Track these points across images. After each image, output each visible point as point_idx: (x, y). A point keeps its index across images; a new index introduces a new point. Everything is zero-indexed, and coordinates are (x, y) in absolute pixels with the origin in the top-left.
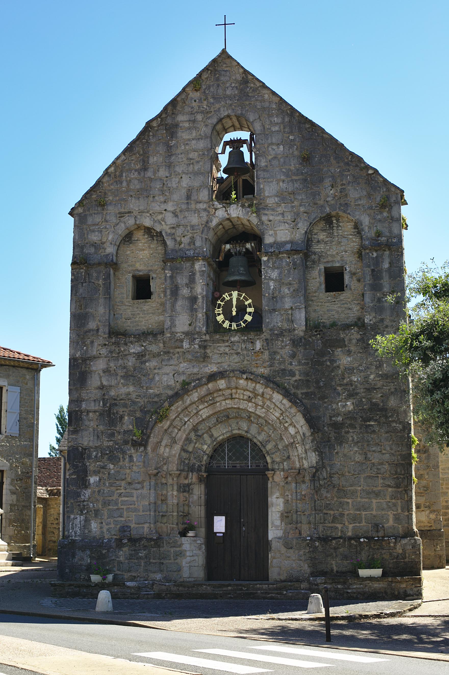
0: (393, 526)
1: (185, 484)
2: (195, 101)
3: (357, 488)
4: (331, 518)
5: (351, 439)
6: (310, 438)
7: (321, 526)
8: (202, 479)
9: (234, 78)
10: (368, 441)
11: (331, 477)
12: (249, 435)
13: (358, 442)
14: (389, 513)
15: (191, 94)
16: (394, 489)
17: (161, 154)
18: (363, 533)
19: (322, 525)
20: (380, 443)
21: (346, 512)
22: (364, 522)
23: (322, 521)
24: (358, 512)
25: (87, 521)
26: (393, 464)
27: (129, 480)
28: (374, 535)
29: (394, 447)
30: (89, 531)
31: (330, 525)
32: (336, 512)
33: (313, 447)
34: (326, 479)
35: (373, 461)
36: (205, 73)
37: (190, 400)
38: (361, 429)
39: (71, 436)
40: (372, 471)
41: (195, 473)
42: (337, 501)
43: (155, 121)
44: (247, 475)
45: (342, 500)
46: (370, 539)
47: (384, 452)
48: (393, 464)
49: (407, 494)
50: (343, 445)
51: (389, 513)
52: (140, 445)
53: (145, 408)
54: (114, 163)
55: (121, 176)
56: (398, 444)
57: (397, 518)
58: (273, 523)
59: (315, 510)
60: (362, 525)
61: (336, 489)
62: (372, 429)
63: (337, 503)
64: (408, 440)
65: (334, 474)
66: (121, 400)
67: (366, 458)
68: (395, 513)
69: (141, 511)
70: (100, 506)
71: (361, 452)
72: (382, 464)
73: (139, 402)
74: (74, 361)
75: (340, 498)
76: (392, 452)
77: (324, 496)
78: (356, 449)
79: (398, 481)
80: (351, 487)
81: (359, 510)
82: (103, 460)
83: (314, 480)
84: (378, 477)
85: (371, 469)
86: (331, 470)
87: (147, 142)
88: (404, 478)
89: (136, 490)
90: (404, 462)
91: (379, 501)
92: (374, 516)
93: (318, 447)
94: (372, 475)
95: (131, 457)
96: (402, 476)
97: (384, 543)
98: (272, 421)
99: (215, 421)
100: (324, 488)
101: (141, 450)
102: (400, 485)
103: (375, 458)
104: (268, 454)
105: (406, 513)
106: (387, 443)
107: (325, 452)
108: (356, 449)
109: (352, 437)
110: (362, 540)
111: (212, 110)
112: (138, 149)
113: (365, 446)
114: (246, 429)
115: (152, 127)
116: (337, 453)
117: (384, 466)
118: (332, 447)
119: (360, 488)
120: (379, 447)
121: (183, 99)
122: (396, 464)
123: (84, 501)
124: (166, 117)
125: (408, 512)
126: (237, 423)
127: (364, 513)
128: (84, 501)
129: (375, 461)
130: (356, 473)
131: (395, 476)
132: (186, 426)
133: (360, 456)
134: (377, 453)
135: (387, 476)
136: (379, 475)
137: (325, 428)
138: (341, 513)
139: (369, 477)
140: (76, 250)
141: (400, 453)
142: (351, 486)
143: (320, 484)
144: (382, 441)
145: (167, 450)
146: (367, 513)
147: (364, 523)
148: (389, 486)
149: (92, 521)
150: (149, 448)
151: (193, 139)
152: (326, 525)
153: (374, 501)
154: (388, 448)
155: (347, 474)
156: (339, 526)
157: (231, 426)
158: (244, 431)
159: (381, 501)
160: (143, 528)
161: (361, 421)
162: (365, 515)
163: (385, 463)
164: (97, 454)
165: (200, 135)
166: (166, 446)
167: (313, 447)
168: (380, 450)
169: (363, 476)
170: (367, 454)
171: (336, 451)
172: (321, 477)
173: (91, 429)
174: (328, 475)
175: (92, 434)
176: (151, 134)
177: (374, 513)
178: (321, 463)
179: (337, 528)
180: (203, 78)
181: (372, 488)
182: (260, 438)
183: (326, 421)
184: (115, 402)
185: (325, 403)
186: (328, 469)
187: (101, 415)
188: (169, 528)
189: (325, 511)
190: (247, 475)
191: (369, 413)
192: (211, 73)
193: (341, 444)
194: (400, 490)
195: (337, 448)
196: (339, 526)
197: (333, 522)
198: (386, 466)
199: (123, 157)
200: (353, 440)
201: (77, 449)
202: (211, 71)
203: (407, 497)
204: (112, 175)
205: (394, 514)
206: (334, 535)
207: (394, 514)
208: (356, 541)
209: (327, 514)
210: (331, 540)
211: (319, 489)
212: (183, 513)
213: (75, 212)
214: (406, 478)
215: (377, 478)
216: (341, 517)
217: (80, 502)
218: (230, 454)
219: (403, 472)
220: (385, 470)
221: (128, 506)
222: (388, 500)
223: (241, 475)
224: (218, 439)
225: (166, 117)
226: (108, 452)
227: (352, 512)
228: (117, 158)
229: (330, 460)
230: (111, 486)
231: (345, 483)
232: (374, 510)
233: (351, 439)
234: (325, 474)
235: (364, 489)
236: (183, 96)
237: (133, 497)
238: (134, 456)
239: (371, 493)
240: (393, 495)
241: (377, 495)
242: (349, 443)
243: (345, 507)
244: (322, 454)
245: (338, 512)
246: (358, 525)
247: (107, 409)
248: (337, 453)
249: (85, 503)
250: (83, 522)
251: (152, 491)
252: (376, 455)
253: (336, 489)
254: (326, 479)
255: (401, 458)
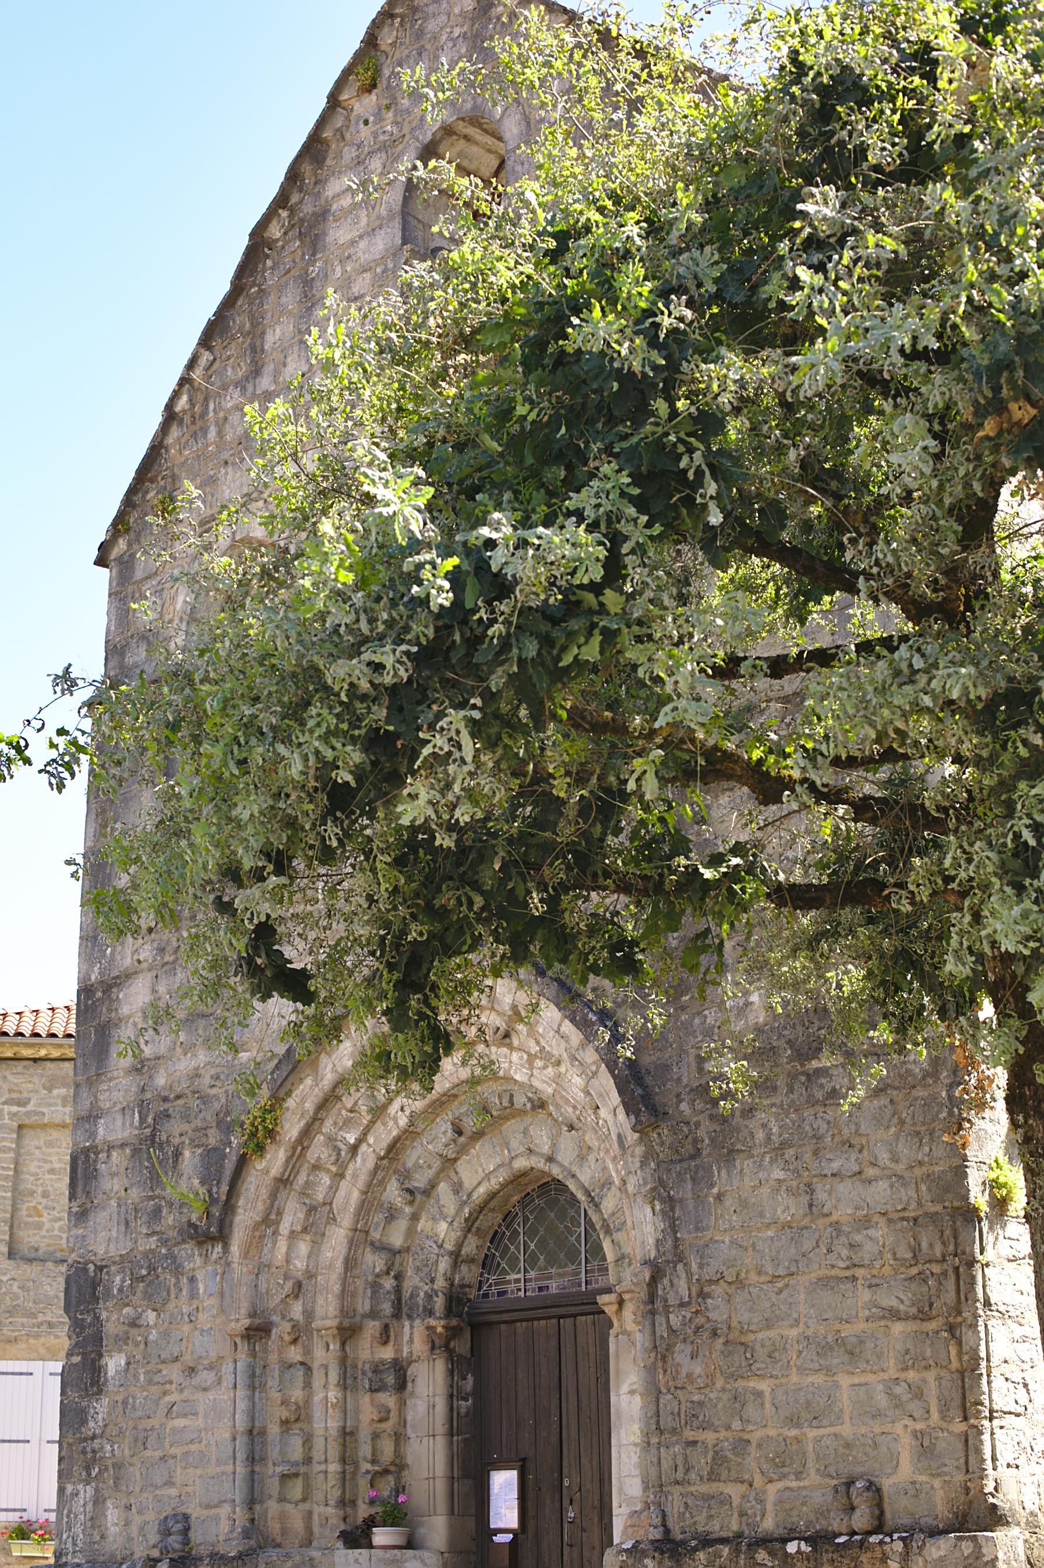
0: (913, 1483)
1: (382, 1362)
2: (366, 123)
3: (786, 1332)
4: (702, 1462)
5: (760, 1135)
6: (639, 1150)
7: (676, 1495)
8: (437, 1341)
9: (457, 11)
10: (818, 1138)
11: (703, 1295)
12: (556, 1171)
13: (784, 1145)
14: (898, 1428)
15: (357, 106)
16: (911, 1326)
17: (290, 312)
18: (812, 1517)
19: (679, 1488)
20: (855, 1141)
21: (756, 1436)
22: (812, 1472)
23: (680, 1475)
24: (794, 1432)
25: (98, 1501)
26: (903, 1219)
27: (187, 1358)
28: (835, 1526)
29: (904, 1149)
30: (103, 1537)
31: (704, 1488)
32: (723, 1434)
33: (645, 1184)
34: (689, 1303)
35: (834, 1218)
36: (386, 30)
37: (334, 1070)
38: (791, 1090)
39: (74, 1232)
40: (832, 1258)
41: (417, 1322)
42: (724, 1389)
43: (274, 222)
44: (575, 1316)
45: (741, 1383)
46: (819, 1540)
47: (870, 1172)
48: (903, 1219)
49: (960, 1344)
50: (738, 1163)
51: (898, 1428)
52: (213, 1239)
53: (228, 1113)
54: (184, 381)
55: (204, 413)
56: (918, 1133)
57: (925, 1449)
58: (621, 1490)
59: (660, 1431)
60: (806, 1483)
61: (721, 1340)
62: (828, 1088)
63: (725, 1397)
64: (951, 1113)
65: (711, 1282)
66: (178, 1097)
67: (811, 1206)
68: (919, 1426)
69: (213, 1461)
70: (127, 1452)
71: (794, 1183)
72: (865, 1223)
73: (216, 1097)
74: (87, 998)
75: (734, 1377)
76: (900, 1168)
77: (684, 1372)
78: (778, 1174)
79: (925, 1289)
80: (769, 1327)
81: (793, 1421)
82: (134, 1299)
83: (653, 1313)
84: (854, 1278)
85: (830, 1251)
86: (701, 1266)
87: (261, 291)
88: (945, 1273)
89: (205, 1390)
90: (938, 1208)
91: (862, 1379)
92: (848, 1446)
93: (661, 1181)
94: (834, 1272)
95: (192, 1280)
96: (936, 1269)
97: (864, 1558)
98: (575, 1108)
99: (450, 1134)
100: (685, 1341)
101: (215, 1256)
102: (931, 1305)
103: (843, 1201)
104: (608, 1232)
105: (959, 1427)
106: (881, 1134)
107: (681, 1200)
108: (778, 1174)
109: (764, 1126)
110: (792, 1547)
111: (406, 130)
112: (240, 320)
113: (808, 1156)
114: (546, 1149)
115: (271, 244)
116: (719, 1197)
117: (871, 1232)
118: (701, 1178)
119: (794, 1333)
120: (854, 1156)
121: (339, 130)
122: (915, 1220)
123: (94, 1437)
124: (301, 202)
125: (966, 1419)
126: (525, 1132)
127: (812, 1434)
128: (94, 1437)
129: (843, 1213)
130: (781, 1271)
131: (914, 1271)
132: (359, 1159)
133: (791, 1202)
134: (848, 1182)
135: (887, 1270)
136: (860, 1272)
137: (684, 1106)
138: (741, 1440)
139: (825, 1282)
140: (111, 664)
141: (924, 1169)
142: (768, 1325)
143: (669, 1327)
144: (863, 1130)
145: (303, 1248)
146: (822, 1432)
147: (812, 1478)
148: (894, 1315)
149: (109, 1503)
150: (235, 1248)
151: (361, 237)
152: (692, 1489)
153: (845, 1381)
154: (884, 1157)
155: (754, 1277)
156: (734, 1491)
157: (507, 1145)
158: (542, 1155)
159: (870, 1378)
160: (217, 1519)
161: (791, 1060)
162: (818, 1440)
163: (876, 1218)
164: (123, 1281)
165: (378, 217)
166: (293, 1235)
167: (645, 1184)
168: (856, 1168)
169: (803, 1280)
170: (813, 1191)
171: (715, 1190)
172: (672, 1300)
173: (113, 1203)
174: (694, 1290)
175: (115, 1216)
176: (269, 263)
177: (846, 1430)
178: (669, 1243)
179: (725, 1501)
180: (383, 48)
181: (837, 1326)
182: (585, 1175)
183: (685, 1080)
184: (166, 1106)
185: (683, 1008)
186: (694, 1267)
187: (136, 1152)
188: (315, 1517)
189: (689, 1434)
190: (575, 1316)
191: (817, 1023)
192: (401, 25)
193: (729, 1156)
194: (932, 1325)
195: (721, 1179)
196: (734, 1491)
197: (713, 1476)
198: (880, 1232)
199: (206, 357)
200: (768, 1139)
201: (85, 1270)
202: (403, 17)
203: (960, 1353)
204: (187, 419)
205: (915, 1434)
206: (717, 1528)
207: (915, 1434)
208: (772, 1554)
209: (694, 1443)
210: (695, 1549)
211: (669, 1348)
212: (373, 1462)
213: (114, 554)
214: (951, 1274)
215: (849, 1285)
216: (737, 1455)
217: (85, 1440)
218: (532, 1246)
219: (938, 1250)
220: (875, 1249)
221: (186, 1448)
222: (893, 1373)
223: (560, 1317)
224: (475, 1196)
225: (301, 202)
226: (144, 1272)
227: (772, 1432)
228: (191, 364)
229: (697, 1229)
230: (150, 1382)
231: (746, 1316)
232: (847, 1419)
233: (760, 1135)
234: (682, 1285)
235: (809, 1333)
236: (338, 121)
237: (196, 1414)
238: (200, 1276)
239: (831, 1349)
240: (907, 1352)
241: (853, 1353)
242: (755, 1152)
243: (751, 1411)
244: (672, 1209)
245: (729, 1434)
246: (794, 1484)
247: (148, 1131)
248: (719, 1197)
249: (96, 1443)
250: (90, 1507)
251: (241, 1393)
252: (844, 1188)
253: (721, 1340)
254: (689, 1303)
255: (929, 1190)
